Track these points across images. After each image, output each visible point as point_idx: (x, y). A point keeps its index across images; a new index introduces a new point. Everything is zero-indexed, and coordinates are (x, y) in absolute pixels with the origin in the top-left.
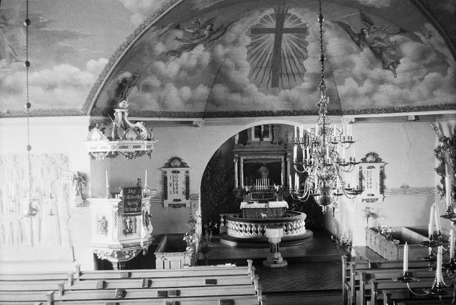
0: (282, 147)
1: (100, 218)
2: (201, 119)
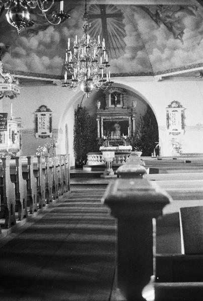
0: (129, 111)
2: (58, 80)
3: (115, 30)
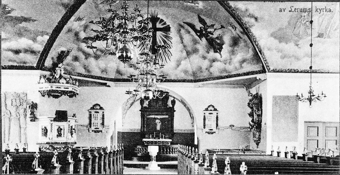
1: (43, 127)
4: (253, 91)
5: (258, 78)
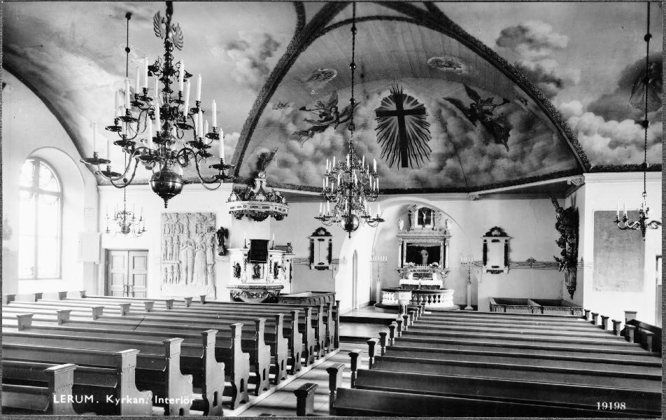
3: (416, 131)
4: (567, 204)
5: (569, 183)
